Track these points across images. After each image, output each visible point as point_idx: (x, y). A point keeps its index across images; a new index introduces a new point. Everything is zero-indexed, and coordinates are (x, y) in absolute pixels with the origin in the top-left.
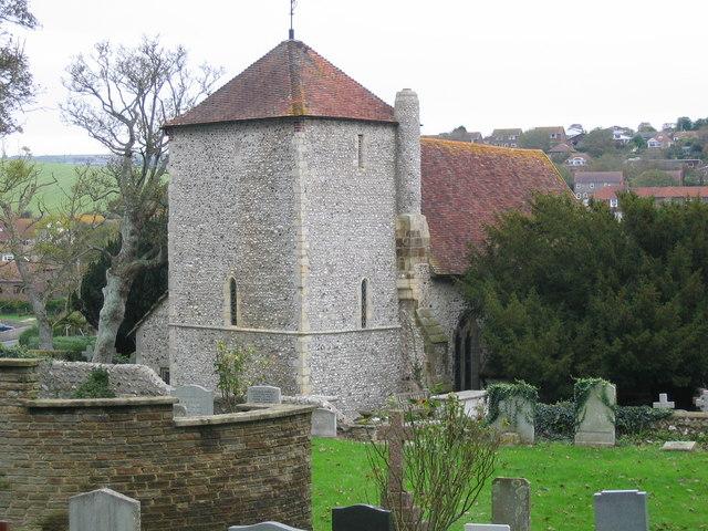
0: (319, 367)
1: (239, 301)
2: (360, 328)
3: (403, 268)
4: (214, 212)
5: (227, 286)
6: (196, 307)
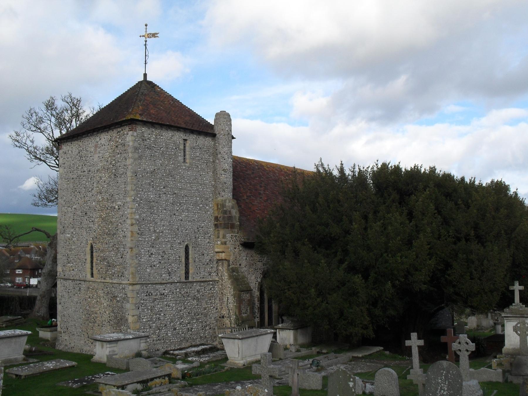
0: (148, 309)
2: (184, 280)
3: (218, 237)
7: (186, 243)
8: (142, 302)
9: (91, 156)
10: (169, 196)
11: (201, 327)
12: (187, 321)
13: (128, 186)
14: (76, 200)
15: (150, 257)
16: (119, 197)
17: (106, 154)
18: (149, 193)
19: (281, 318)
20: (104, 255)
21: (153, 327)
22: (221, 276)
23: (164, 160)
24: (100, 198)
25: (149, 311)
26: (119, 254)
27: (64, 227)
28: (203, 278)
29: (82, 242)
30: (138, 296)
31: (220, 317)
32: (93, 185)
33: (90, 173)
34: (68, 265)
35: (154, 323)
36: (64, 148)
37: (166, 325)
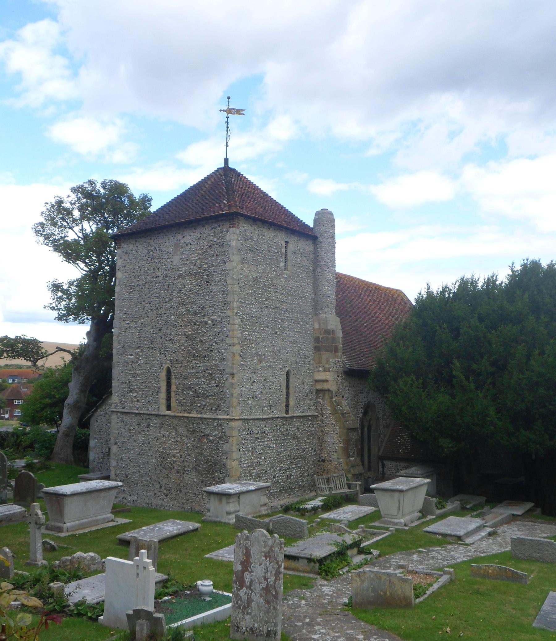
0: (249, 451)
1: (173, 388)
3: (320, 362)
4: (154, 308)
5: (163, 375)
6: (135, 394)
7: (287, 369)
8: (243, 442)
9: (168, 258)
11: (300, 474)
13: (228, 296)
14: (144, 312)
15: (252, 385)
16: (213, 309)
17: (193, 255)
19: (382, 462)
20: (189, 382)
22: (321, 410)
23: (266, 266)
24: (183, 310)
25: (250, 454)
26: (213, 382)
28: (303, 412)
29: (152, 366)
30: (240, 434)
31: (319, 461)
32: (171, 294)
33: (167, 279)
34: (129, 394)
35: (254, 469)
36: (125, 246)
37: (266, 471)
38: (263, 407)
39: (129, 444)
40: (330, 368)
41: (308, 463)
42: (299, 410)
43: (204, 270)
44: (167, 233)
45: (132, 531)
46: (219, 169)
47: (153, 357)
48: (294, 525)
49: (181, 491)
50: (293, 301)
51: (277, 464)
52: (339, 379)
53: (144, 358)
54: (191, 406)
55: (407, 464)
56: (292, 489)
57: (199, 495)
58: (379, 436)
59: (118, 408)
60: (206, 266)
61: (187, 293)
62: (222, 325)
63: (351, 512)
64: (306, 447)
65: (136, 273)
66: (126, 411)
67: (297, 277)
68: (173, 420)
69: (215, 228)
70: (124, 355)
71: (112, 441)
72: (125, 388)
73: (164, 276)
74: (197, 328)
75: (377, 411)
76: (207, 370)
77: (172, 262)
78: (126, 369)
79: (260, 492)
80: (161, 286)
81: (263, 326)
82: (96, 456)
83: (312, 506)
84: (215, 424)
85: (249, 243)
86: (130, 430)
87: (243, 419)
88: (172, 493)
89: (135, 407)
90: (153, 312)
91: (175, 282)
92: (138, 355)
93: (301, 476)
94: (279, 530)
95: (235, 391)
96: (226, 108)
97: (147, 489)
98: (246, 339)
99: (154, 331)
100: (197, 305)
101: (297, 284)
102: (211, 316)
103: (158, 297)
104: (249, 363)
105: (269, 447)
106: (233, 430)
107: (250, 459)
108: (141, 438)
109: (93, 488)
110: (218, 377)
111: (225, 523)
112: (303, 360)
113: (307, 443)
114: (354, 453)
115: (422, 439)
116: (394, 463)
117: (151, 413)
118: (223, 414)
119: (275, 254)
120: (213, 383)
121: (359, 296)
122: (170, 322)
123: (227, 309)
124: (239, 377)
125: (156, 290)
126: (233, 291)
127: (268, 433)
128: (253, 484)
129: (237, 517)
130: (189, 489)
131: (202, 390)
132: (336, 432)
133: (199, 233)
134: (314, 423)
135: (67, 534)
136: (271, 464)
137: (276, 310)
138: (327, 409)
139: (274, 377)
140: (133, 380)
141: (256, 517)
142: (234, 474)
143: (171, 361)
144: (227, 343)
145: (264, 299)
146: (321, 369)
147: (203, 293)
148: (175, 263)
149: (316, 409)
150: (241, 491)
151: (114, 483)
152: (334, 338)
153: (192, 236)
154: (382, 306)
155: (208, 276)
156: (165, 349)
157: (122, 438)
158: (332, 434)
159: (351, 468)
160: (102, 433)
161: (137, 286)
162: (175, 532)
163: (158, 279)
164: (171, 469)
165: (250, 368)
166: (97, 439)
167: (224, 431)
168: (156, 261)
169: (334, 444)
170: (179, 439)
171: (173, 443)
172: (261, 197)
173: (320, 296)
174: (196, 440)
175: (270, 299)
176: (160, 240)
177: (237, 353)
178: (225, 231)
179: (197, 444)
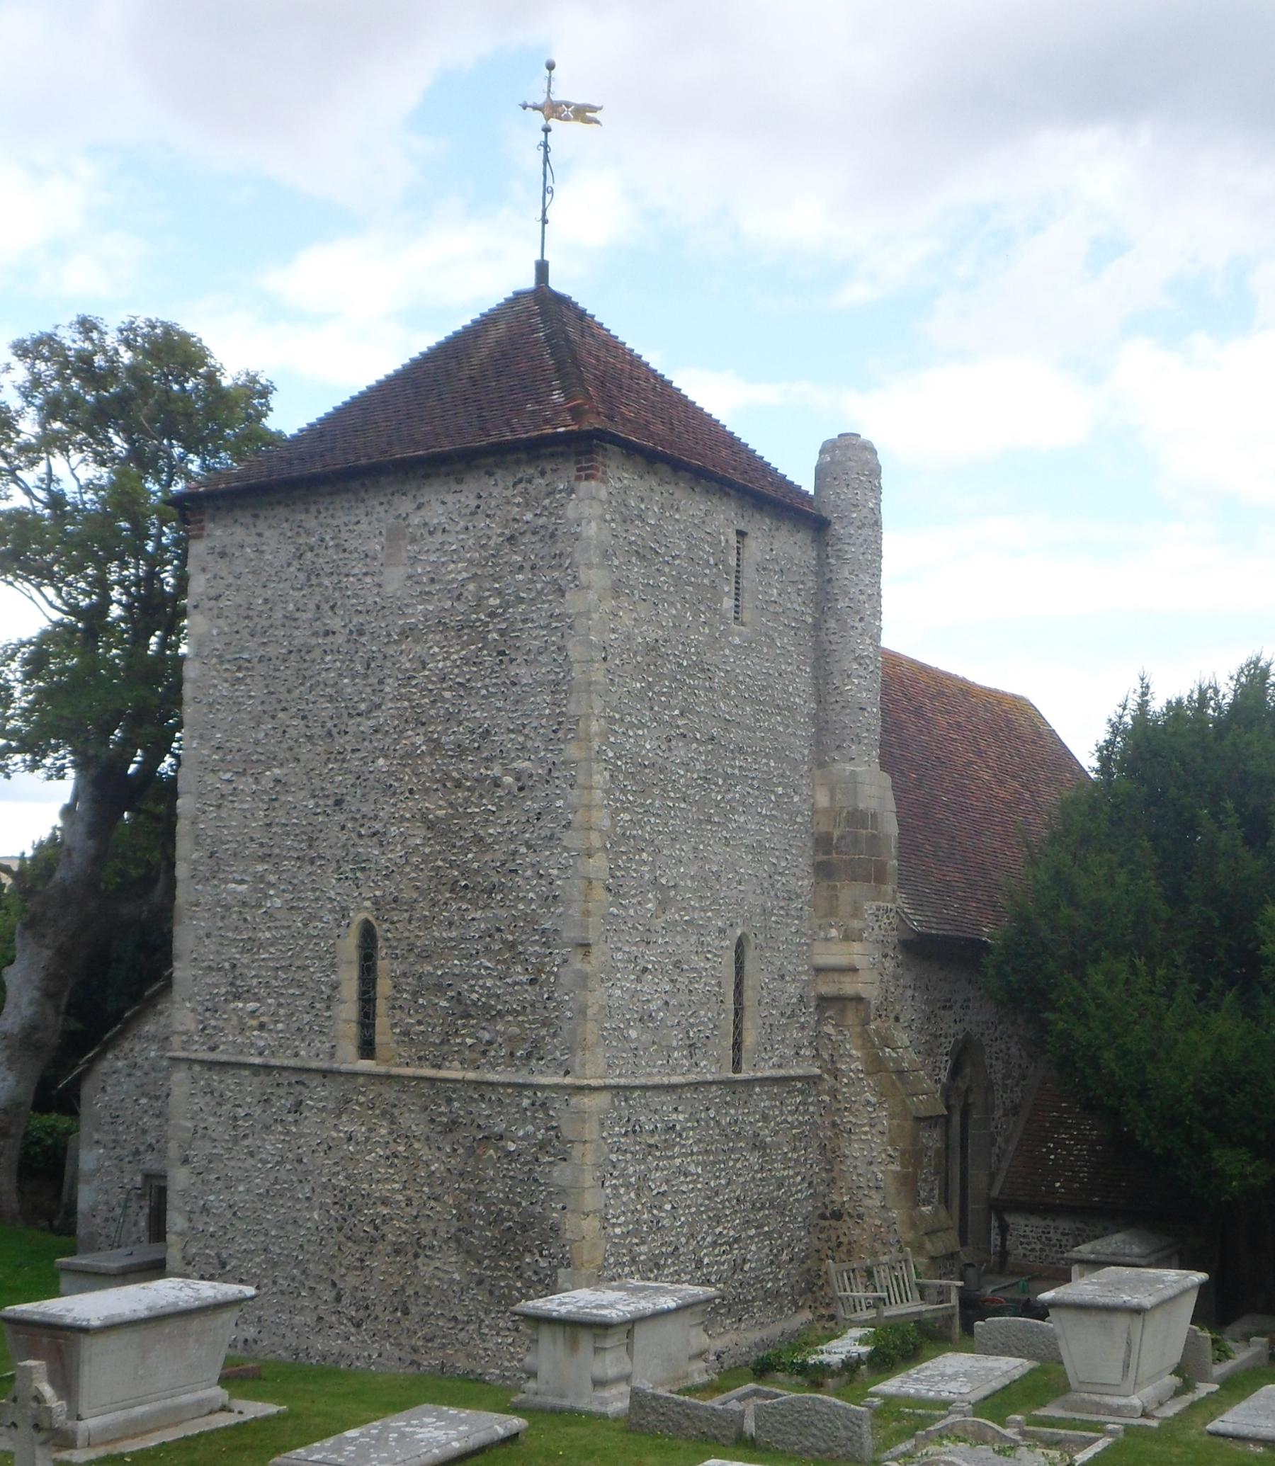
0: (628, 1186)
1: (384, 987)
3: (832, 912)
4: (317, 731)
5: (349, 946)
6: (252, 1006)
7: (739, 932)
8: (614, 1157)
9: (366, 574)
10: (695, 745)
11: (768, 1255)
12: (732, 1233)
14: (285, 746)
15: (639, 980)
16: (521, 739)
17: (452, 566)
18: (640, 732)
20: (436, 968)
21: (642, 1258)
24: (419, 740)
25: (632, 1195)
26: (519, 969)
27: (212, 855)
28: (780, 1066)
29: (312, 917)
30: (605, 1134)
32: (377, 687)
33: (363, 639)
34: (232, 1006)
35: (643, 1243)
36: (218, 533)
37: (676, 1249)
38: (671, 1049)
39: (232, 1163)
40: (862, 930)
41: (790, 1222)
42: (771, 1058)
43: (492, 615)
44: (362, 494)
45: (317, 1444)
46: (518, 296)
47: (314, 890)
48: (831, 1421)
49: (406, 1312)
50: (758, 720)
51: (706, 1226)
52: (887, 965)
53: (284, 891)
54: (442, 1043)
55: (1081, 1226)
56: (747, 1302)
57: (468, 1322)
58: (993, 1142)
59: (195, 1047)
60: (498, 601)
61: (430, 687)
62: (549, 789)
63: (965, 1374)
64: (786, 1173)
65: (256, 620)
66: (224, 1058)
67: (769, 647)
68: (383, 1089)
69: (530, 481)
70: (216, 882)
71: (173, 1150)
72: (217, 986)
73: (351, 632)
74: (467, 800)
75: (987, 1062)
76: (499, 930)
77: (380, 586)
78: (220, 924)
79: (688, 1313)
80: (343, 662)
81: (672, 794)
82: (101, 1198)
83: (843, 1357)
84: (526, 1103)
85: (636, 532)
86: (235, 1118)
87: (617, 1087)
88: (376, 1318)
89: (252, 1044)
90: (315, 745)
91: (390, 651)
92: (262, 882)
93: (772, 1262)
94: (779, 1436)
95: (591, 999)
96: (540, 99)
97: (292, 1303)
98: (624, 834)
99: (317, 805)
100: (466, 724)
101: (768, 668)
102: (513, 760)
103: (331, 699)
104: (632, 912)
105: (686, 1175)
106: (584, 1122)
107: (633, 1213)
108: (272, 1145)
109: (169, 1305)
110: (538, 955)
111: (589, 1414)
112: (782, 904)
113: (790, 1159)
114: (932, 1190)
115: (1157, 1151)
116: (1035, 1221)
117: (307, 1066)
118: (549, 1071)
119: (707, 571)
120: (519, 973)
121: (919, 712)
122: (372, 776)
123: (566, 741)
124: (604, 954)
125: (324, 674)
126: (590, 684)
127: (684, 1129)
128: (667, 1292)
129: (636, 1394)
130: (436, 1305)
131: (481, 995)
132: (879, 1128)
133: (472, 496)
134: (810, 1100)
135: (92, 1454)
136: (691, 1225)
137: (710, 747)
138: (850, 1056)
139: (702, 957)
140: (245, 959)
141: (679, 1392)
142: (585, 1258)
143: (376, 902)
144: (565, 849)
145: (677, 712)
146: (834, 933)
147: (486, 687)
148: (389, 589)
149: (817, 1056)
150: (638, 1315)
151: (231, 1290)
152: (874, 837)
153: (450, 505)
154: (983, 743)
155: (502, 633)
156: (356, 863)
157: (209, 1145)
158: (866, 1133)
159: (926, 1238)
160: (121, 1129)
161: (260, 661)
162: (456, 1445)
163: (330, 639)
164: (374, 1241)
165: (634, 928)
166: (105, 1147)
167: (554, 1124)
168: (326, 582)
169: (871, 1163)
170: (401, 1148)
171: (382, 1161)
172: (654, 389)
173: (834, 706)
174: (461, 1151)
175: (692, 711)
176: (339, 513)
177: (598, 879)
178: (561, 491)
179: (461, 1166)
